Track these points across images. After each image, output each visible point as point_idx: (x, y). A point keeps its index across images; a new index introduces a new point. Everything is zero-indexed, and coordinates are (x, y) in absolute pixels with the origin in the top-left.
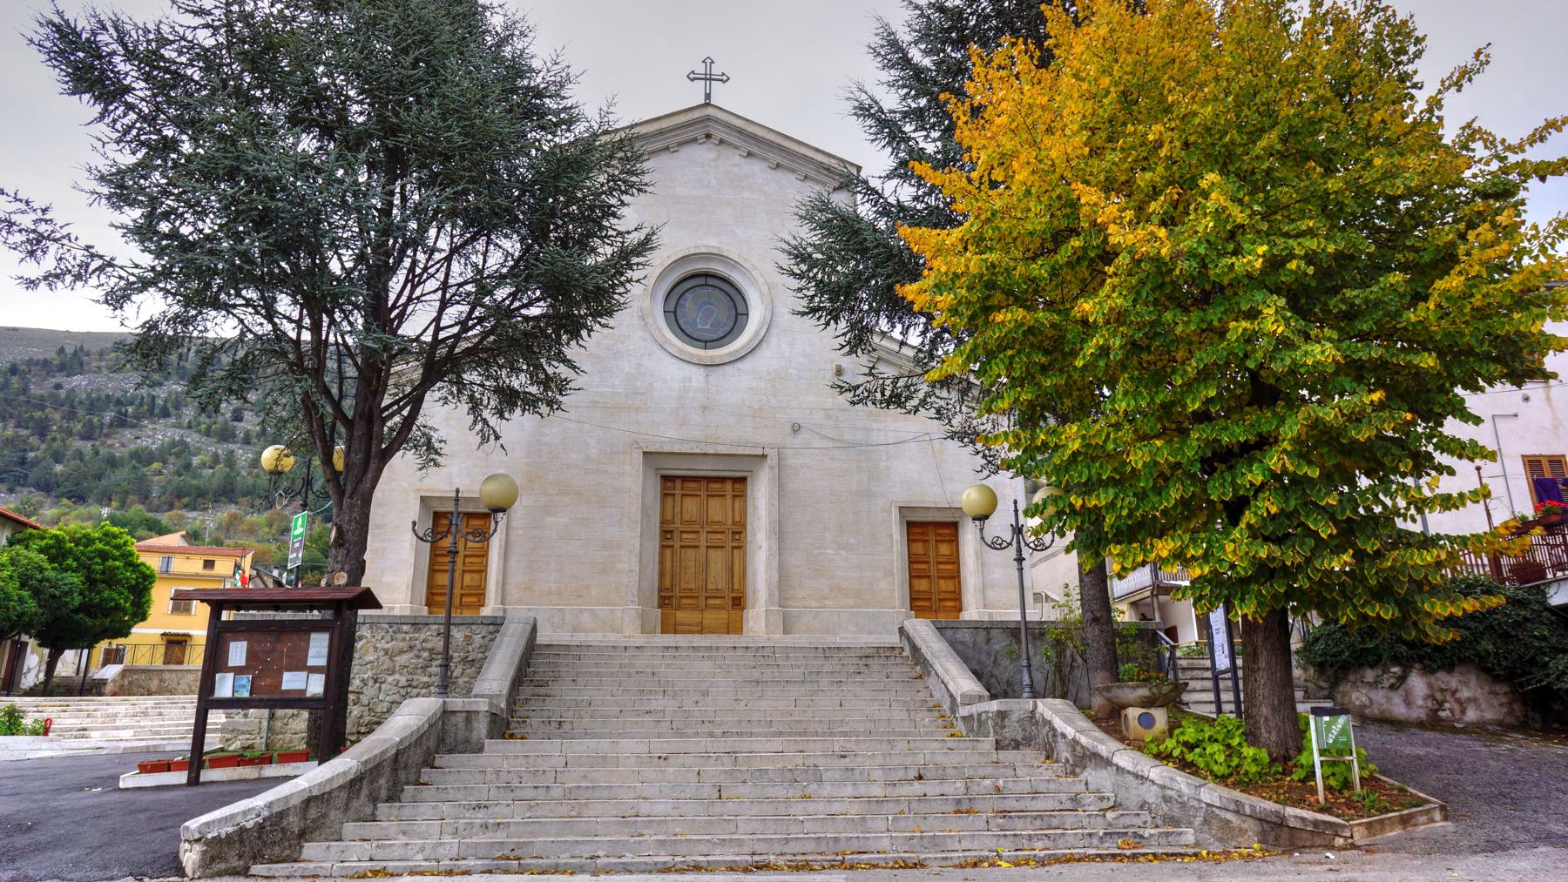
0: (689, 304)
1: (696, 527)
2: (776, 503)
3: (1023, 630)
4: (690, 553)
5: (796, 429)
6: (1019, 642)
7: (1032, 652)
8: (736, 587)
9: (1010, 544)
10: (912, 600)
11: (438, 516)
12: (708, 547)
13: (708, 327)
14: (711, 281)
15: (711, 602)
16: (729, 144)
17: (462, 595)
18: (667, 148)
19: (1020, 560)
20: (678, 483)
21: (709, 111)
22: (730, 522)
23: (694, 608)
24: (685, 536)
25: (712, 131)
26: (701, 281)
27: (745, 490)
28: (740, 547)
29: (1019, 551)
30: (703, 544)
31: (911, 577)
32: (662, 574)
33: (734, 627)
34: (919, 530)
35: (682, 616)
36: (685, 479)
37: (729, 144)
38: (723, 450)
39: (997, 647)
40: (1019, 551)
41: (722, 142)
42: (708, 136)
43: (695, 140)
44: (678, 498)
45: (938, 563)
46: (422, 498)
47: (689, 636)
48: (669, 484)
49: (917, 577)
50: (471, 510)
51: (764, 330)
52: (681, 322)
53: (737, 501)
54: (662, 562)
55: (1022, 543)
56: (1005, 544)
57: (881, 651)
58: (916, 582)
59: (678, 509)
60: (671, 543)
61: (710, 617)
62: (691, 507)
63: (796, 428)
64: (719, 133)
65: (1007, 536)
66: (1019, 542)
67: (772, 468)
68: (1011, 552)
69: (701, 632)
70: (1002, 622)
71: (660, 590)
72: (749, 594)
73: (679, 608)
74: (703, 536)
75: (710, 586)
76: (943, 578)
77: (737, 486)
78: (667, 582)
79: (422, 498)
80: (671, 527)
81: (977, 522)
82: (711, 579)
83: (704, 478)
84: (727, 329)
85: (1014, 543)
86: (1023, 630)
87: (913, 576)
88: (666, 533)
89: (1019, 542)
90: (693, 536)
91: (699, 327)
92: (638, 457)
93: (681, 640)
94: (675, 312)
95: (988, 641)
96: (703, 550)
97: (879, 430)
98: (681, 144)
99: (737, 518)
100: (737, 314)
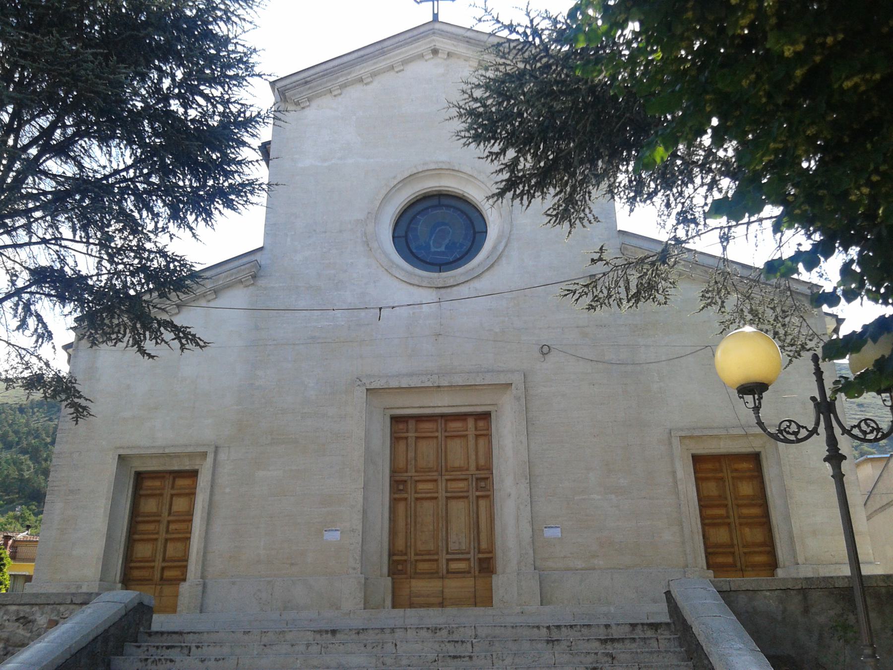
0: (422, 227)
1: (434, 476)
2: (524, 439)
3: (858, 593)
4: (427, 505)
5: (545, 351)
6: (854, 610)
7: (876, 624)
8: (484, 545)
9: (814, 431)
10: (708, 555)
11: (140, 477)
12: (447, 498)
13: (443, 249)
14: (445, 201)
15: (454, 566)
16: (459, 56)
17: (448, 560)
18: (392, 68)
19: (835, 457)
20: (412, 424)
21: (437, 26)
22: (473, 466)
23: (433, 575)
24: (421, 486)
25: (439, 45)
26: (435, 202)
27: (489, 428)
28: (487, 497)
29: (832, 442)
30: (442, 494)
31: (704, 525)
32: (393, 533)
33: (483, 599)
34: (709, 466)
35: (420, 586)
36: (419, 418)
37: (459, 56)
38: (459, 380)
39: (822, 619)
40: (832, 442)
41: (449, 55)
42: (435, 52)
43: (421, 56)
44: (412, 441)
45: (739, 506)
46: (120, 457)
47: (422, 611)
48: (401, 426)
49: (714, 525)
50: (176, 468)
51: (503, 244)
52: (413, 246)
53: (482, 442)
54: (393, 519)
55: (837, 431)
56: (803, 433)
57: (639, 629)
58: (712, 531)
59: (411, 454)
60: (405, 495)
61: (453, 586)
62: (427, 452)
63: (545, 349)
64: (445, 45)
65: (807, 418)
66: (829, 428)
67: (518, 399)
68: (818, 445)
69: (442, 605)
70: (825, 579)
71: (391, 554)
72: (499, 553)
73: (417, 575)
74: (442, 485)
75: (453, 547)
76: (747, 524)
77: (481, 424)
78: (400, 544)
79: (120, 457)
80: (403, 476)
81: (749, 398)
82: (453, 537)
83: (442, 416)
84: (465, 249)
85: (822, 429)
86: (858, 593)
87: (707, 523)
88: (398, 484)
89: (829, 428)
90: (430, 486)
91: (433, 249)
92: (360, 394)
93: (411, 616)
94: (406, 236)
95: (806, 611)
96: (442, 502)
97: (646, 346)
98: (405, 62)
99: (482, 462)
100: (475, 233)
